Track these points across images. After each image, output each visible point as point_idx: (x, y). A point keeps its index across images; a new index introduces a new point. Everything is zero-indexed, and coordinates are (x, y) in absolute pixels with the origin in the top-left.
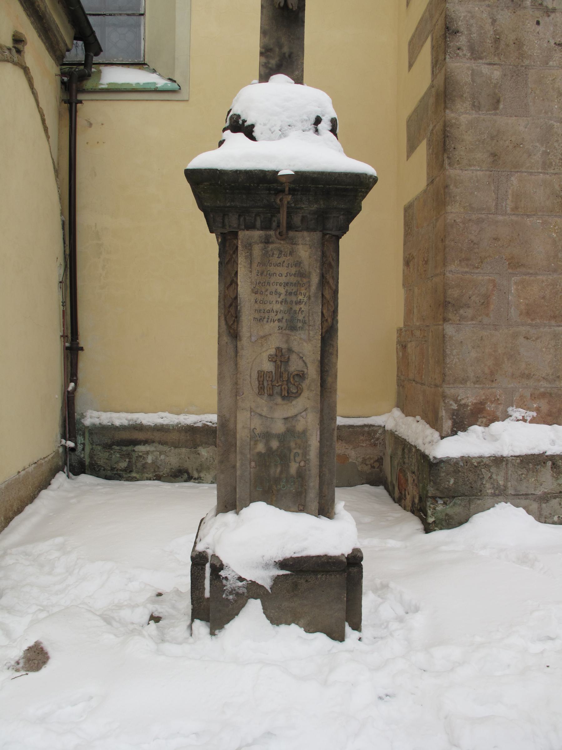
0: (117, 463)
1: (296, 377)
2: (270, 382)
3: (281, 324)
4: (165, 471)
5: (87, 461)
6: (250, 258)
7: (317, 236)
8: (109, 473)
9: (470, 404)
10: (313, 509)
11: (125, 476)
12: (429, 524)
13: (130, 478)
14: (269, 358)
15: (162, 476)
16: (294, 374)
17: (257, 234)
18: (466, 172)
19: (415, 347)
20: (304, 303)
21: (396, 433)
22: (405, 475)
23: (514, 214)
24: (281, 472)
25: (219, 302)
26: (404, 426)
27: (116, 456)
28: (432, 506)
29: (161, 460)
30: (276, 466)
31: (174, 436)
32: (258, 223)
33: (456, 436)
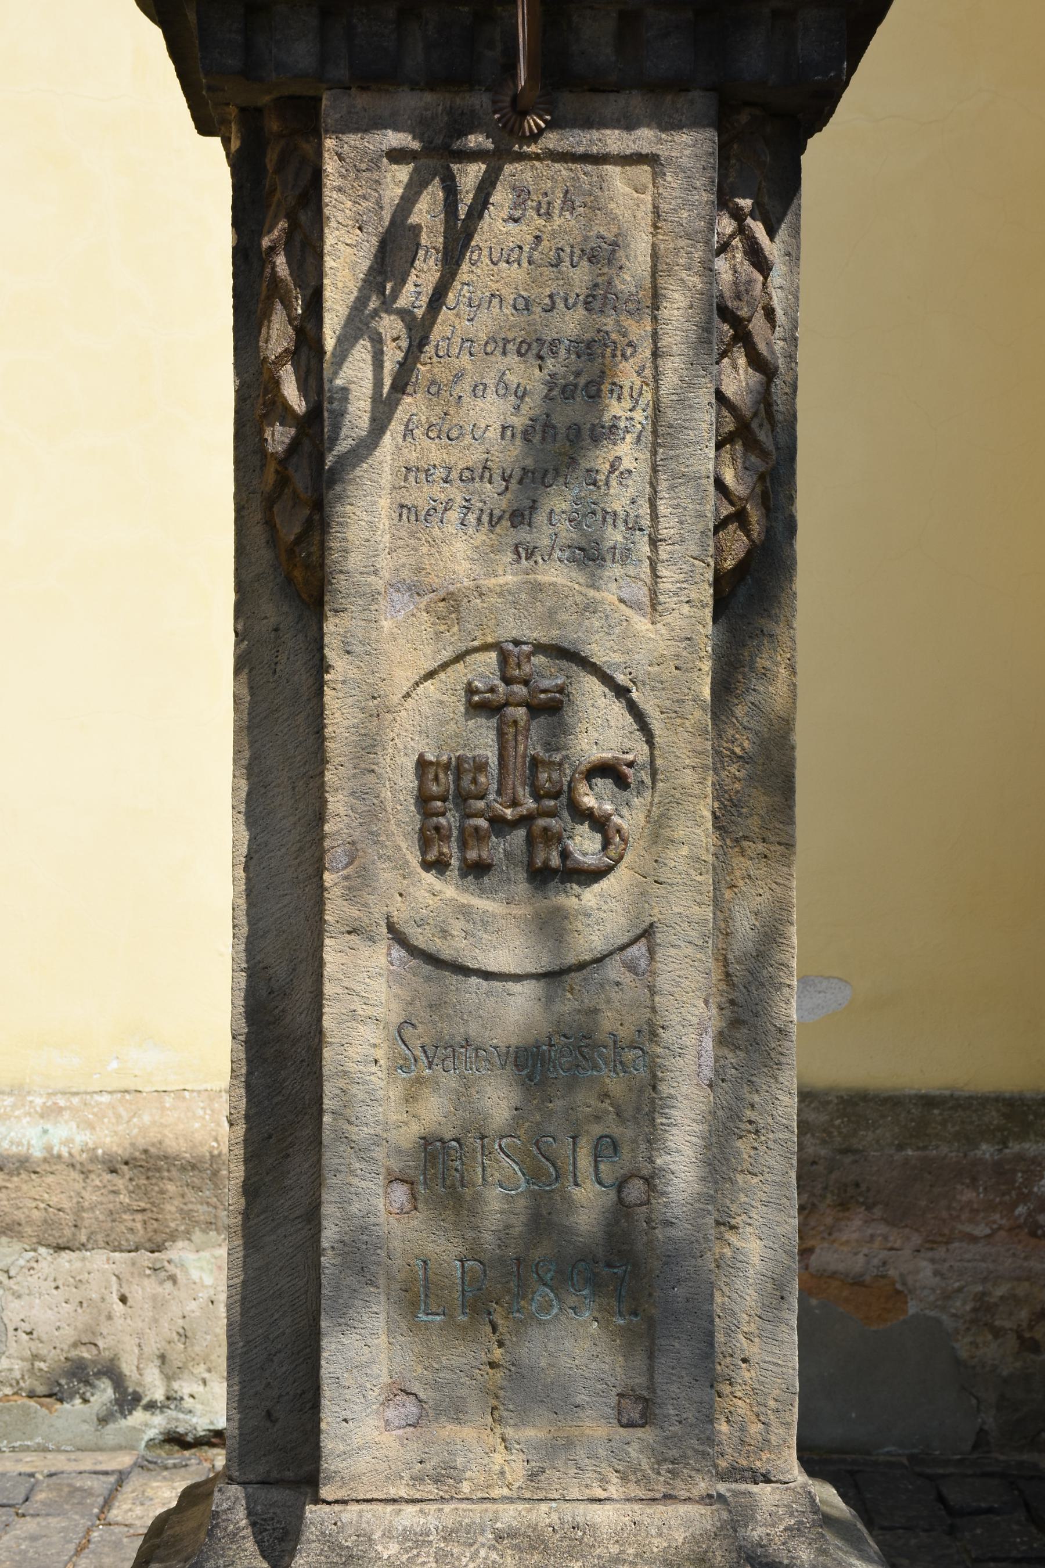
31: (59, 1192)
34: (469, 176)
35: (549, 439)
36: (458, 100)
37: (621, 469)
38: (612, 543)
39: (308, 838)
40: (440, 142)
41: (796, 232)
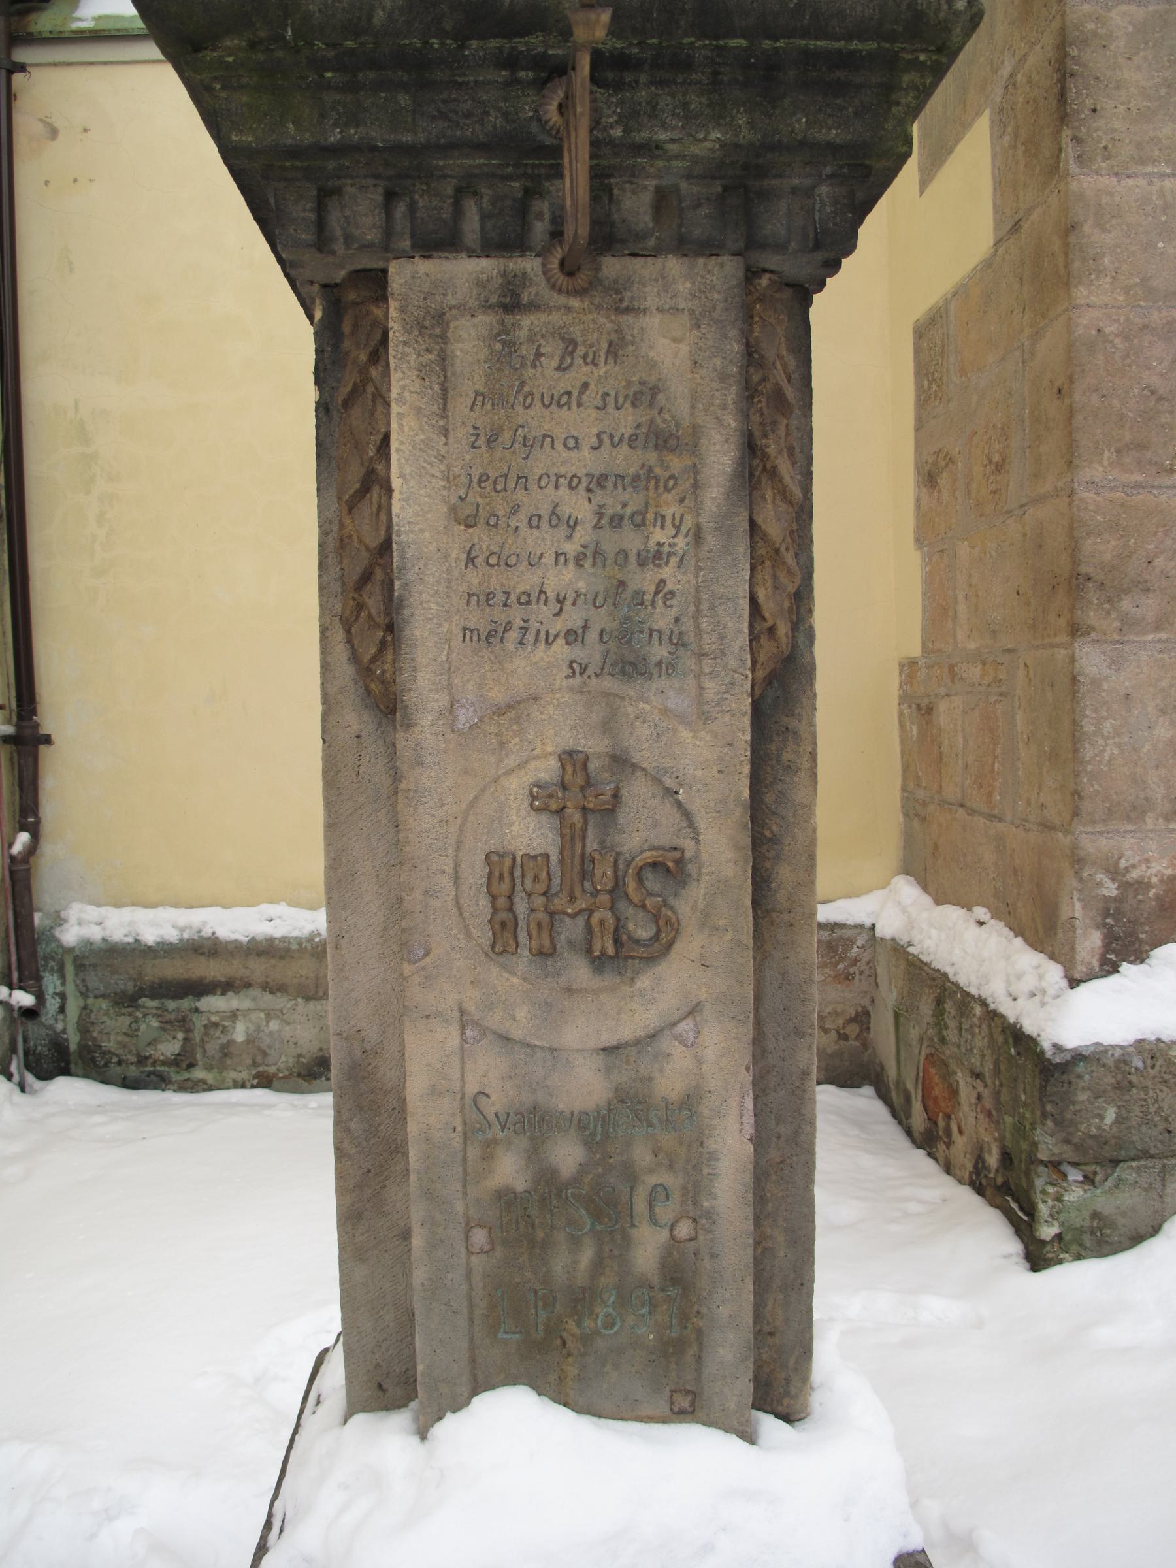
0: (153, 1043)
1: (649, 875)
2: (539, 901)
3: (578, 653)
4: (282, 1061)
5: (73, 1040)
6: (440, 374)
7: (722, 272)
8: (133, 1071)
9: (1154, 880)
10: (732, 1405)
11: (175, 1077)
12: (1043, 1243)
13: (190, 1084)
14: (534, 798)
15: (275, 1075)
16: (639, 861)
17: (465, 273)
18: (1131, 182)
19: (965, 712)
20: (674, 560)
21: (910, 949)
22: (947, 1075)
24: (598, 1266)
25: (322, 566)
26: (934, 933)
27: (149, 1026)
28: (1050, 1190)
29: (271, 1033)
30: (575, 1242)
32: (471, 225)
33: (1114, 978)
35: (599, 564)
36: (511, 265)
37: (666, 590)
38: (659, 658)
39: (392, 919)
40: (494, 301)
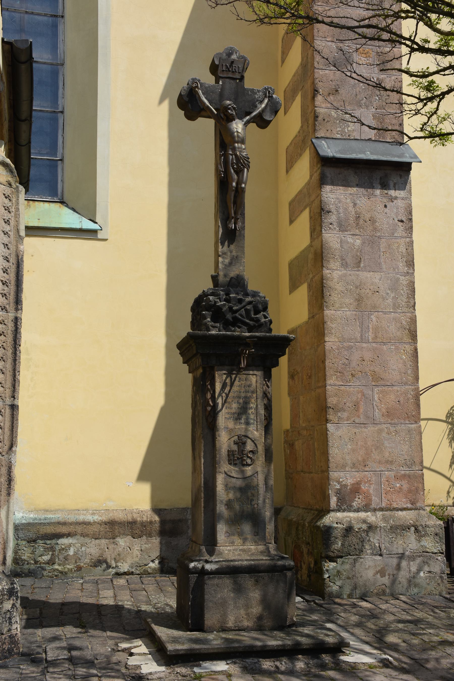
9: (349, 484)
23: (374, 342)
27: (40, 550)
31: (96, 529)
34: (234, 376)
41: (271, 383)
